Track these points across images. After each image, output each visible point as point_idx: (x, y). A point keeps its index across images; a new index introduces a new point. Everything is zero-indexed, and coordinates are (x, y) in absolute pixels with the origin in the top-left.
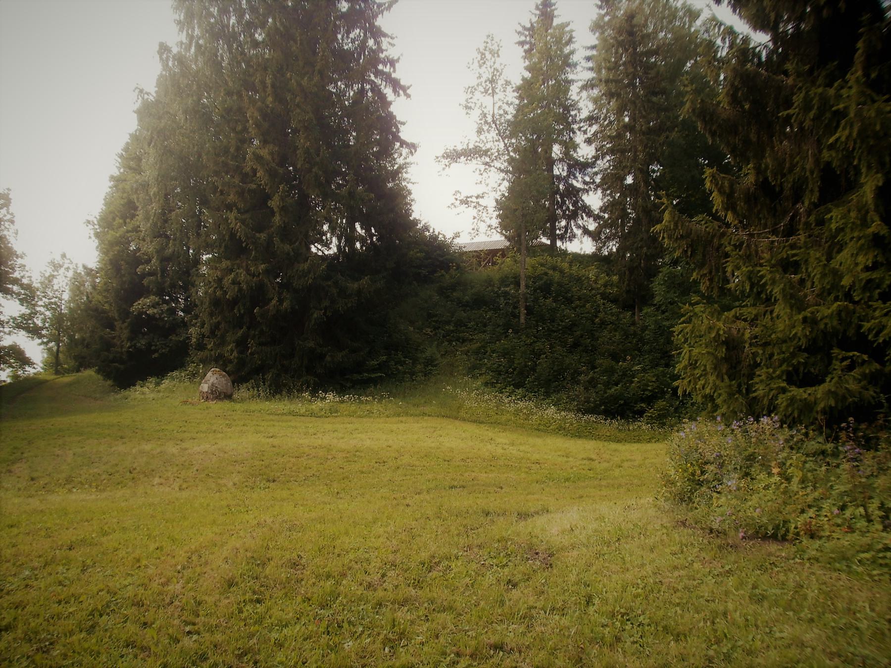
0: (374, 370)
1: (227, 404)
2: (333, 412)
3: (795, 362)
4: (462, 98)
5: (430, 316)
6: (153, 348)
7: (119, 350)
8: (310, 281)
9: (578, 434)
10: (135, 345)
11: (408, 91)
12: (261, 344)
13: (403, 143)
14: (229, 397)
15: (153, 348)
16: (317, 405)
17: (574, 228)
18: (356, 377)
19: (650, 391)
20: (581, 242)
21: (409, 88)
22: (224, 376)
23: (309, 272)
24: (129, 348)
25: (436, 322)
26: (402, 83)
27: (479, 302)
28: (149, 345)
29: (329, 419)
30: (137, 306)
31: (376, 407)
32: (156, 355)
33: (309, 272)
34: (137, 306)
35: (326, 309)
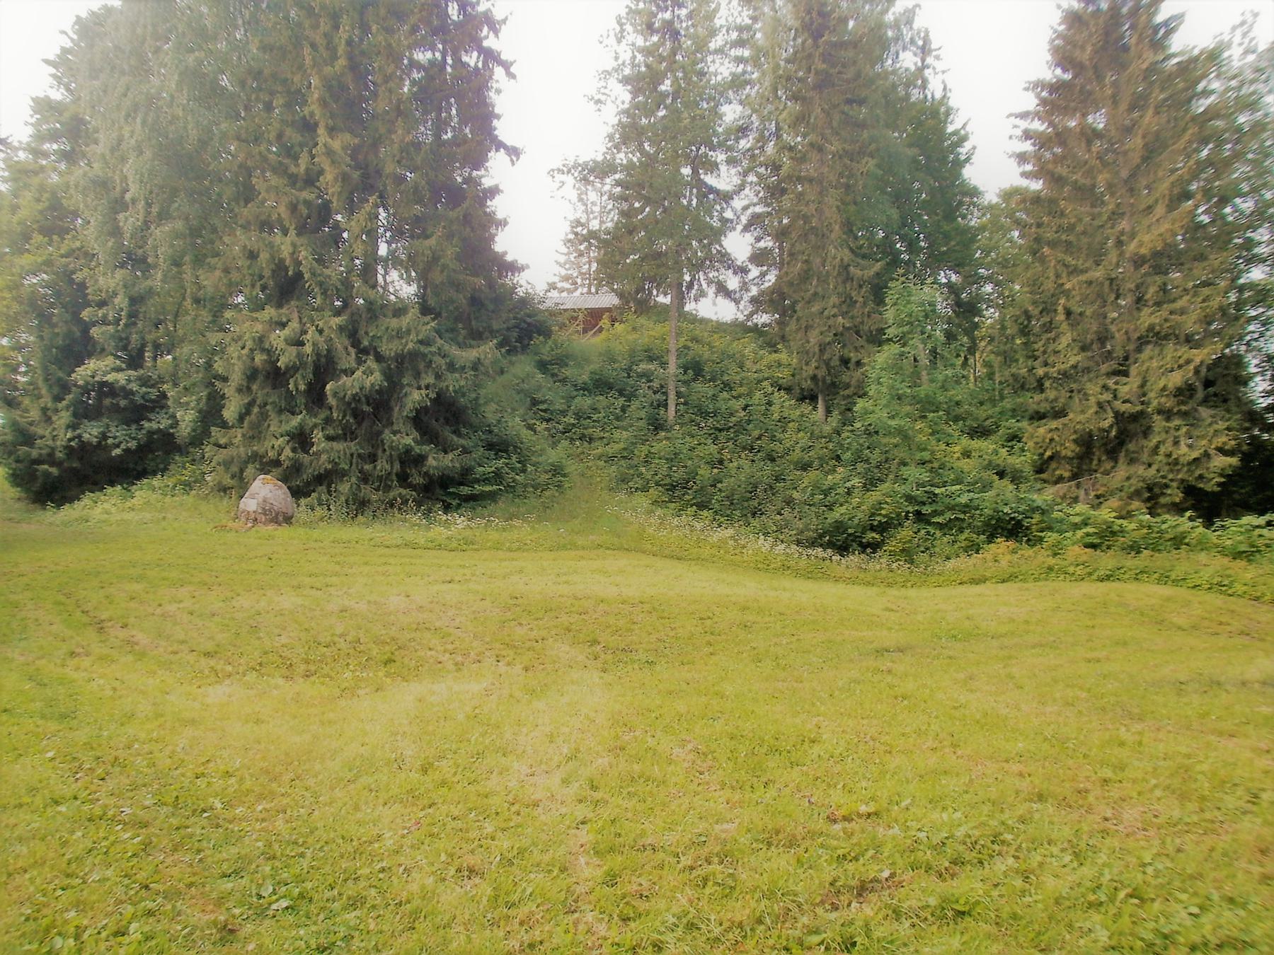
0: (486, 480)
1: (283, 532)
2: (467, 544)
3: (848, 485)
4: (592, 86)
5: (535, 402)
6: (110, 441)
7: (50, 443)
8: (410, 345)
9: (808, 575)
10: (79, 436)
11: (512, 69)
12: (329, 438)
13: (500, 145)
14: (288, 519)
15: (110, 441)
16: (438, 532)
17: (703, 283)
18: (465, 490)
19: (884, 516)
20: (714, 304)
21: (512, 64)
22: (280, 487)
23: (409, 332)
24: (70, 440)
25: (545, 411)
26: (503, 57)
27: (601, 385)
28: (104, 436)
29: (468, 553)
30: (82, 374)
31: (522, 531)
32: (117, 452)
33: (409, 332)
34: (82, 374)
35: (427, 387)
